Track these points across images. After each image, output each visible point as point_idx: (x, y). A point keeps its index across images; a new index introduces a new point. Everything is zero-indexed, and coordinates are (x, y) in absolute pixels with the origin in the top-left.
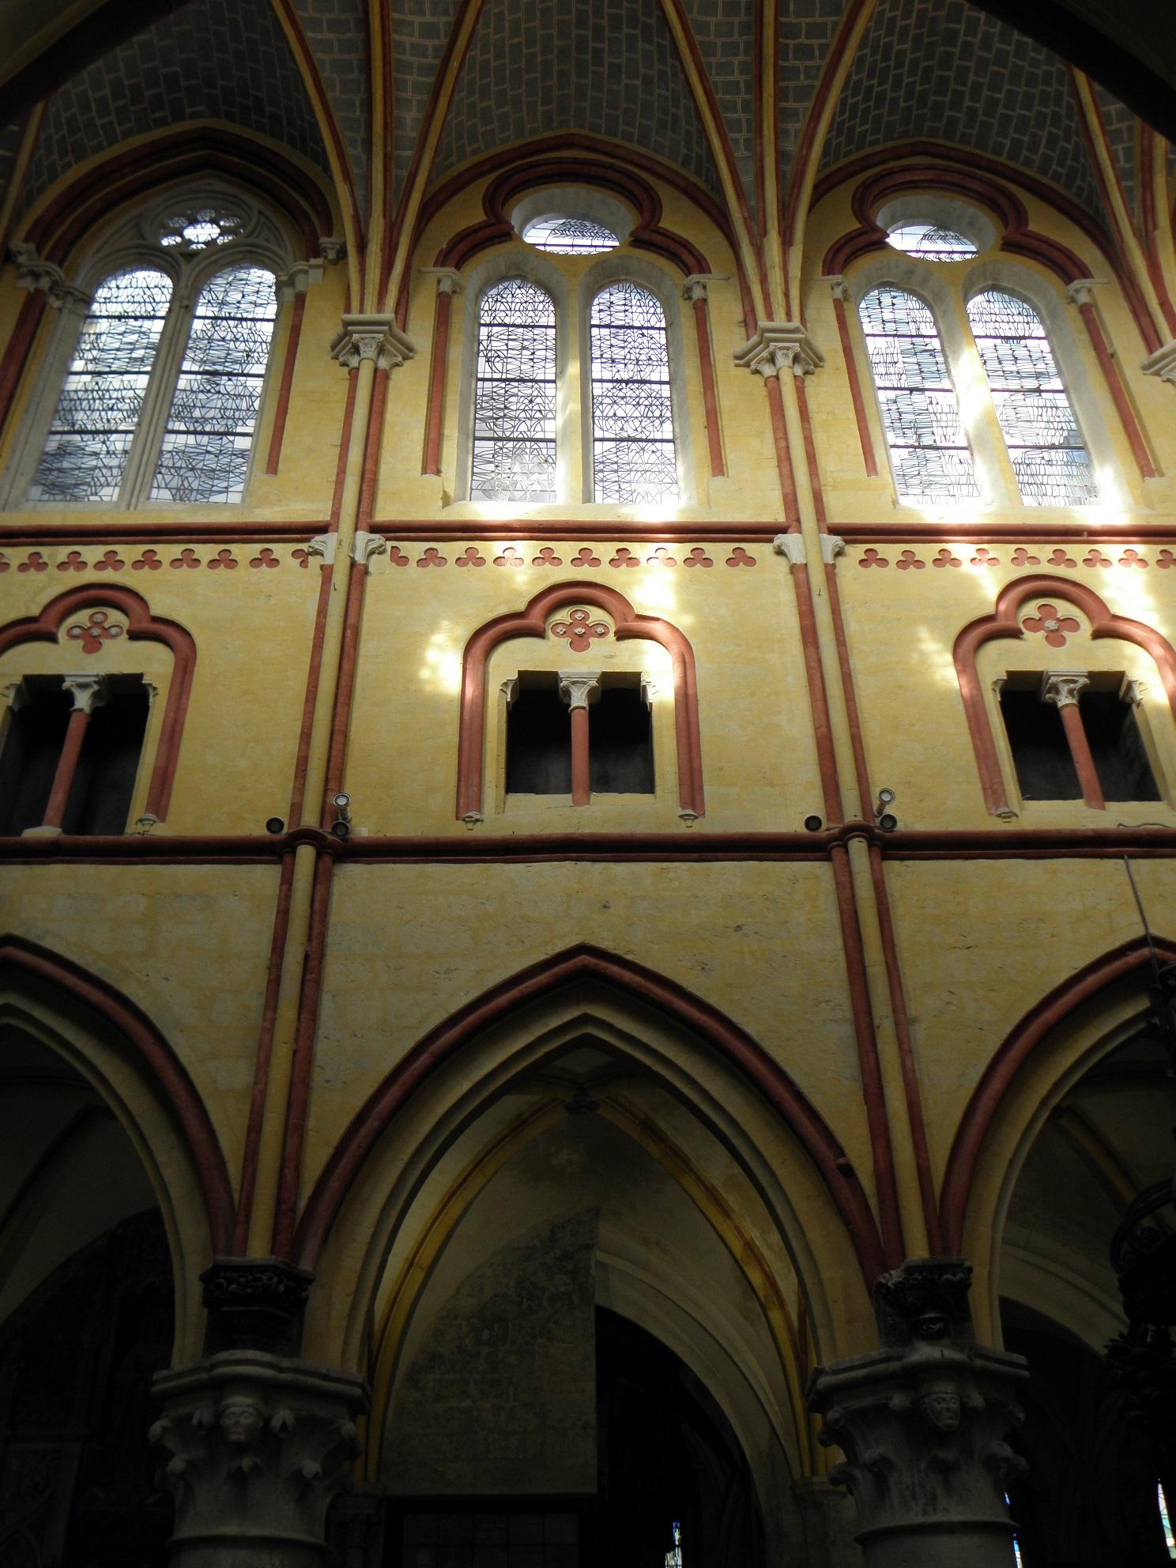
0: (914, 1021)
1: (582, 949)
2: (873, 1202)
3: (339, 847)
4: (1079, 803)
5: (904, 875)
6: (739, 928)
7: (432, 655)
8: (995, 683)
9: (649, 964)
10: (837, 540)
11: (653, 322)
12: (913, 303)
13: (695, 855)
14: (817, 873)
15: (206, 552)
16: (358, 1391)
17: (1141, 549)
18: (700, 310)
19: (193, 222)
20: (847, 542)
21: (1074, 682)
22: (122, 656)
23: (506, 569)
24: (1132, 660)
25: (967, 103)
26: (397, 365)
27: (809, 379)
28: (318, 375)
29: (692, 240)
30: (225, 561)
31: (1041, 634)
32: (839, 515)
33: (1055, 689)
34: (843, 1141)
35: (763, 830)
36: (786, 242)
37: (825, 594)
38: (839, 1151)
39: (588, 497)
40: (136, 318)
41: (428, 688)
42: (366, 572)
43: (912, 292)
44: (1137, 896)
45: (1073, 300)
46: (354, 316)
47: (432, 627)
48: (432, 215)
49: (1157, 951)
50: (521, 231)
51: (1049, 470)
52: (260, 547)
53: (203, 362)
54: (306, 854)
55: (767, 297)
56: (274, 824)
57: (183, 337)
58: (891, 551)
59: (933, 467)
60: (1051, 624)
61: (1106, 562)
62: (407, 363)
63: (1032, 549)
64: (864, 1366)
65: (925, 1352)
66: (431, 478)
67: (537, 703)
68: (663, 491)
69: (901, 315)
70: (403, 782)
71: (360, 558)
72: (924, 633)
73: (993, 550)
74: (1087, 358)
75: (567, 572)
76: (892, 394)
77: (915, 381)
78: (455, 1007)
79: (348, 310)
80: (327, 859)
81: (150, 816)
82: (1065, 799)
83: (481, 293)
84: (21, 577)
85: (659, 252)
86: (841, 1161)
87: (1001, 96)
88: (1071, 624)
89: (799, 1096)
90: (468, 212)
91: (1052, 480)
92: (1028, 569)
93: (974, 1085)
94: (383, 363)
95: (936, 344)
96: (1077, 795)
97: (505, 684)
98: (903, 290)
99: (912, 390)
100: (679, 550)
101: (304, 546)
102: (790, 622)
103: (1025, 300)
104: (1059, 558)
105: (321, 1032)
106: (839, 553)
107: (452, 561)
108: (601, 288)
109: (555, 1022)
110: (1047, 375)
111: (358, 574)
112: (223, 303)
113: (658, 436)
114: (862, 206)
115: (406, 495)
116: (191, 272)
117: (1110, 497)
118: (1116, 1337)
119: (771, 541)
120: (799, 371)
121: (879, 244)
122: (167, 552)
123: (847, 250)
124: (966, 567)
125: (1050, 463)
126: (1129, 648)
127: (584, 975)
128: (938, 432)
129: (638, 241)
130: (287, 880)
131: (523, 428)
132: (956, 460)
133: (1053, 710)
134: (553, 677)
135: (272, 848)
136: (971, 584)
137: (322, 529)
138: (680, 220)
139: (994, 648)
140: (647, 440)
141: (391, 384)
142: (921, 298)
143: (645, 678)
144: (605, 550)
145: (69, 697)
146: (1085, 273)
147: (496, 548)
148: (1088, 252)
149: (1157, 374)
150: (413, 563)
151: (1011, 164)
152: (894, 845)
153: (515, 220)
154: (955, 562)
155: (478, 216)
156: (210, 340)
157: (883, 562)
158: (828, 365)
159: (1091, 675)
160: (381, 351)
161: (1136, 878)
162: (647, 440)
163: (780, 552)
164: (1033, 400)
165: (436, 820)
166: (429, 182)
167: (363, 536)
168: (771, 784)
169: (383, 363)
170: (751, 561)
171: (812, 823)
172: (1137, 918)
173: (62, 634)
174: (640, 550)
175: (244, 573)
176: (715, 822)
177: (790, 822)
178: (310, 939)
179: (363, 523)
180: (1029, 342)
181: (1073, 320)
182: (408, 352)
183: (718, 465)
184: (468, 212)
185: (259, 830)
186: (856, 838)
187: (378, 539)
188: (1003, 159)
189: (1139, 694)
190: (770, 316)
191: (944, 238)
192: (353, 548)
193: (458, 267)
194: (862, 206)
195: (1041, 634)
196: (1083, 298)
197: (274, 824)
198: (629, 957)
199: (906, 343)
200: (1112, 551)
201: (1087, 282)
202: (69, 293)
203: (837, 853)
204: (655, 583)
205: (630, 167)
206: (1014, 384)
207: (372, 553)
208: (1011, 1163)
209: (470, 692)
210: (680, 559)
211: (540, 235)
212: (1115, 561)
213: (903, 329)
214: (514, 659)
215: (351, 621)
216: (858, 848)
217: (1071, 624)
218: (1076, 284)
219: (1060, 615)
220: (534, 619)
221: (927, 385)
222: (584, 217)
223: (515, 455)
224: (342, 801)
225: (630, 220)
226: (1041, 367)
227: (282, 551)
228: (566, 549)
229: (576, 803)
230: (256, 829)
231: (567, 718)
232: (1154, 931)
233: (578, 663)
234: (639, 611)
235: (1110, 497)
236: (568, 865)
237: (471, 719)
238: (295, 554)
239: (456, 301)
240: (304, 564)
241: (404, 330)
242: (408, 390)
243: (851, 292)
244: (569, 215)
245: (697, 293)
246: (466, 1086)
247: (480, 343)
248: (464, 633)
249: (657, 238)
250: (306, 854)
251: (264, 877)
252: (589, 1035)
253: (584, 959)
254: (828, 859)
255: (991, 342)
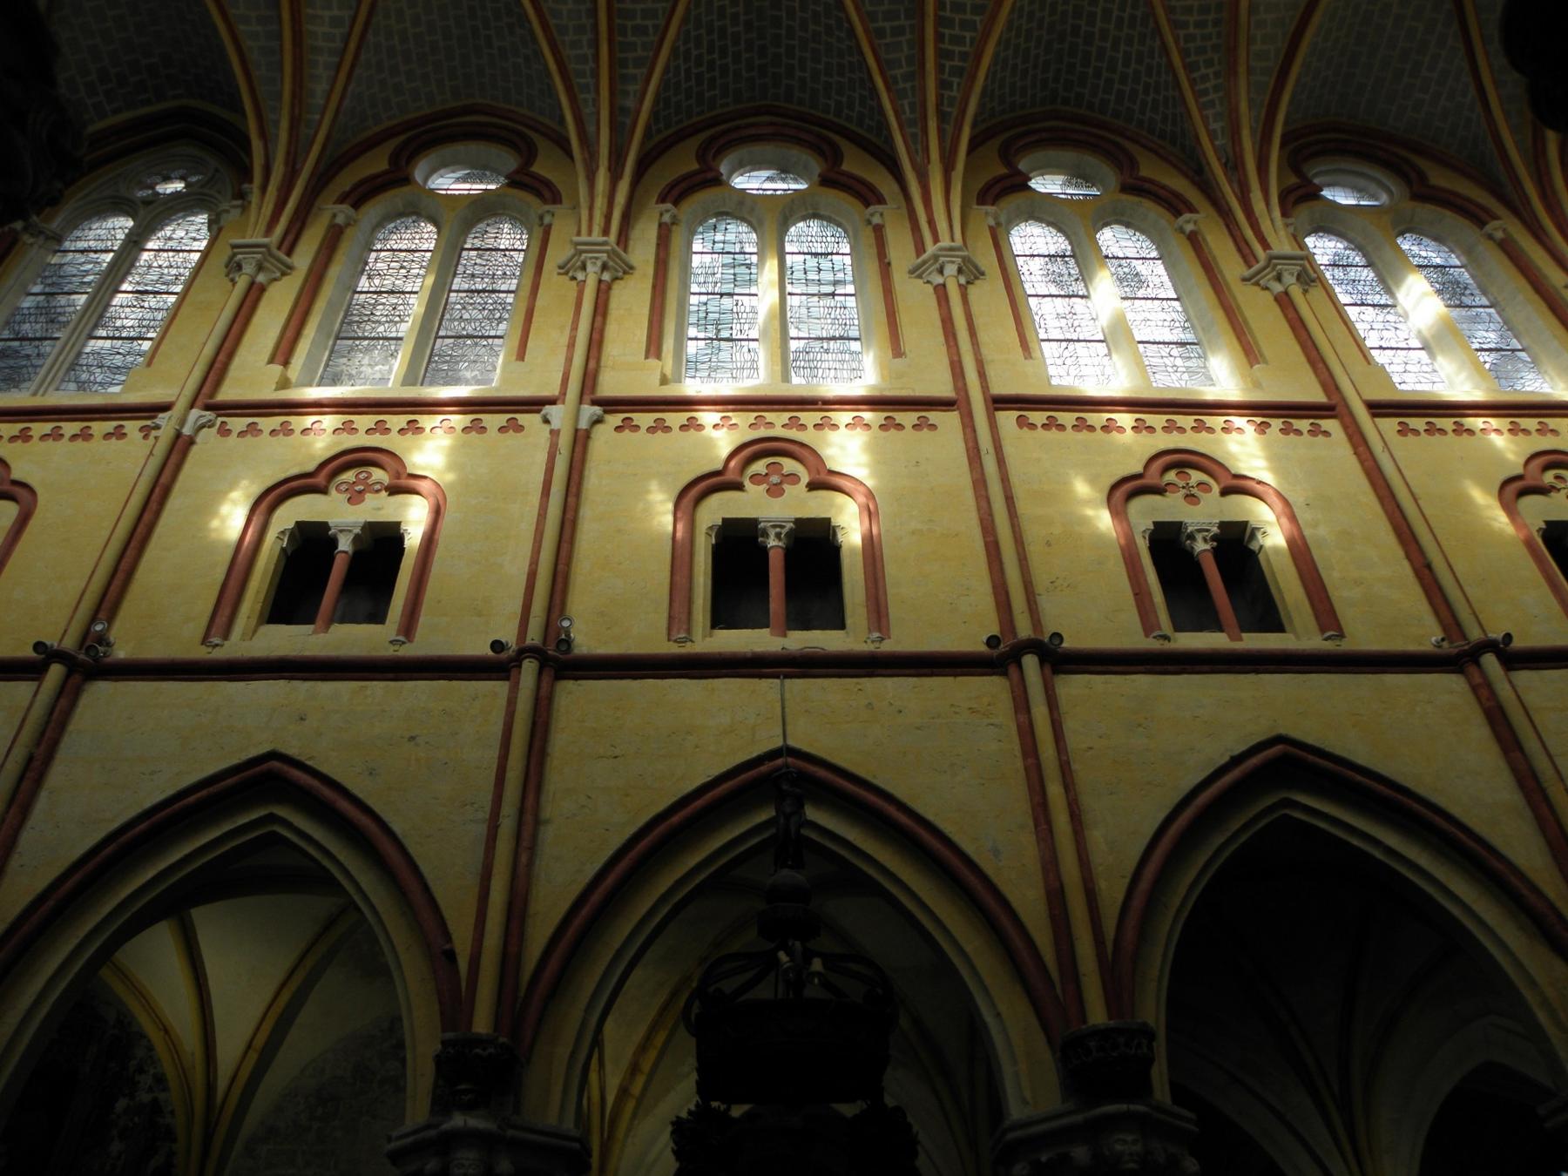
0: (547, 822)
1: (273, 755)
2: (464, 984)
3: (560, 662)
4: (765, 631)
5: (1072, 687)
6: (412, 738)
7: (225, 509)
8: (711, 528)
9: (324, 769)
10: (598, 410)
11: (517, 245)
12: (744, 228)
13: (391, 675)
14: (992, 688)
15: (70, 428)
16: (577, 1145)
17: (868, 416)
18: (879, 231)
19: (167, 179)
20: (605, 412)
21: (782, 527)
22: (798, 504)
23: (310, 438)
24: (840, 509)
25: (798, 73)
26: (275, 280)
27: (970, 287)
28: (555, 288)
29: (554, 180)
30: (85, 435)
31: (764, 486)
32: (1000, 388)
33: (765, 534)
34: (452, 927)
35: (307, 653)
36: (615, 178)
37: (992, 450)
38: (448, 937)
39: (786, 378)
40: (96, 252)
41: (213, 535)
42: (191, 442)
43: (743, 220)
44: (783, 708)
45: (869, 222)
46: (584, 238)
47: (232, 486)
48: (646, 169)
49: (790, 760)
50: (730, 176)
51: (825, 356)
52: (115, 423)
53: (138, 283)
54: (1030, 662)
55: (931, 223)
56: (497, 646)
57: (127, 264)
58: (644, 419)
59: (724, 355)
60: (775, 479)
61: (835, 426)
62: (285, 279)
63: (770, 416)
64: (415, 1132)
65: (458, 1121)
66: (653, 362)
67: (738, 547)
68: (865, 374)
69: (730, 237)
70: (166, 611)
71: (187, 431)
72: (654, 485)
73: (736, 417)
74: (872, 267)
75: (361, 440)
76: (704, 298)
77: (728, 288)
78: (148, 804)
79: (579, 234)
80: (77, 678)
81: (401, 638)
82: (753, 628)
83: (380, 225)
84: (43, 445)
85: (531, 192)
86: (447, 947)
87: (821, 67)
88: (793, 478)
89: (426, 888)
90: (683, 162)
91: (826, 365)
92: (762, 432)
93: (587, 880)
94: (606, 277)
95: (754, 259)
96: (764, 624)
97: (283, 532)
98: (737, 218)
99: (722, 295)
100: (458, 420)
101: (148, 423)
102: (539, 477)
103: (839, 225)
104: (794, 423)
105: (30, 823)
106: (598, 421)
107: (676, 428)
108: (480, 220)
109: (242, 820)
110: (844, 282)
111: (581, 440)
112: (170, 239)
113: (492, 333)
114: (1007, 155)
115: (625, 373)
116: (152, 216)
117: (1222, 378)
118: (684, 1115)
119: (538, 412)
120: (963, 280)
121: (717, 181)
122: (39, 428)
123: (997, 188)
124: (708, 431)
125: (827, 351)
126: (840, 498)
127: (784, 780)
128: (736, 327)
129: (826, 181)
130: (514, 690)
131: (381, 329)
132: (745, 350)
133: (764, 551)
134: (324, 526)
135: (996, 660)
136: (710, 444)
137: (552, 401)
138: (855, 164)
139: (716, 499)
140: (482, 337)
141: (267, 294)
142: (750, 224)
143: (403, 527)
144: (396, 421)
145: (333, 542)
146: (881, 200)
147: (308, 421)
148: (886, 186)
149: (920, 277)
150: (235, 434)
151: (836, 120)
152: (1061, 660)
153: (723, 169)
154: (700, 427)
155: (383, 165)
156: (150, 267)
157: (1061, 427)
158: (637, 274)
159: (798, 521)
160: (604, 267)
161: (787, 696)
162: (482, 337)
163: (546, 421)
164: (829, 302)
165: (651, 639)
166: (643, 144)
167: (590, 411)
168: (480, 615)
169: (606, 277)
170: (933, 427)
171: (992, 641)
172: (780, 731)
173: (747, 483)
174: (427, 421)
175: (97, 446)
176: (901, 641)
177: (972, 641)
178: (38, 743)
179: (201, 401)
180: (835, 257)
181: (868, 235)
182: (629, 269)
183: (898, 352)
184: (375, 163)
185: (484, 650)
186: (1025, 655)
187: (209, 415)
188: (831, 117)
189: (840, 538)
190: (936, 240)
191: (783, 180)
192: (183, 422)
193: (676, 203)
194: (1007, 155)
195: (764, 486)
196: (876, 220)
197: (497, 646)
198: (309, 763)
199: (728, 259)
200: (843, 417)
201: (879, 208)
202: (41, 232)
203: (1012, 670)
204: (848, 448)
205: (520, 127)
206: (813, 289)
207: (202, 426)
208: (619, 954)
209: (679, 534)
210: (459, 428)
211: (741, 182)
212: (1159, 429)
213: (729, 248)
214: (717, 509)
215: (163, 480)
216: (1030, 662)
217: (793, 478)
218: (872, 209)
219: (785, 471)
220: (320, 480)
221: (737, 290)
222: (485, 167)
223: (367, 350)
224: (566, 624)
225: (816, 167)
226: (840, 276)
227: (132, 427)
228: (364, 421)
229: (315, 632)
230: (480, 648)
231: (332, 559)
232: (791, 743)
233: (773, 507)
234: (410, 470)
235: (1222, 378)
236: (282, 682)
237: (242, 559)
238: (141, 429)
239: (349, 232)
240: (146, 437)
241: (625, 250)
242: (631, 299)
243: (1003, 219)
244: (472, 167)
245: (547, 220)
246: (150, 873)
247: (366, 263)
248: (256, 489)
249: (527, 180)
250: (529, 667)
251: (494, 691)
252: (275, 833)
253: (276, 764)
254: (1005, 674)
255: (802, 257)
